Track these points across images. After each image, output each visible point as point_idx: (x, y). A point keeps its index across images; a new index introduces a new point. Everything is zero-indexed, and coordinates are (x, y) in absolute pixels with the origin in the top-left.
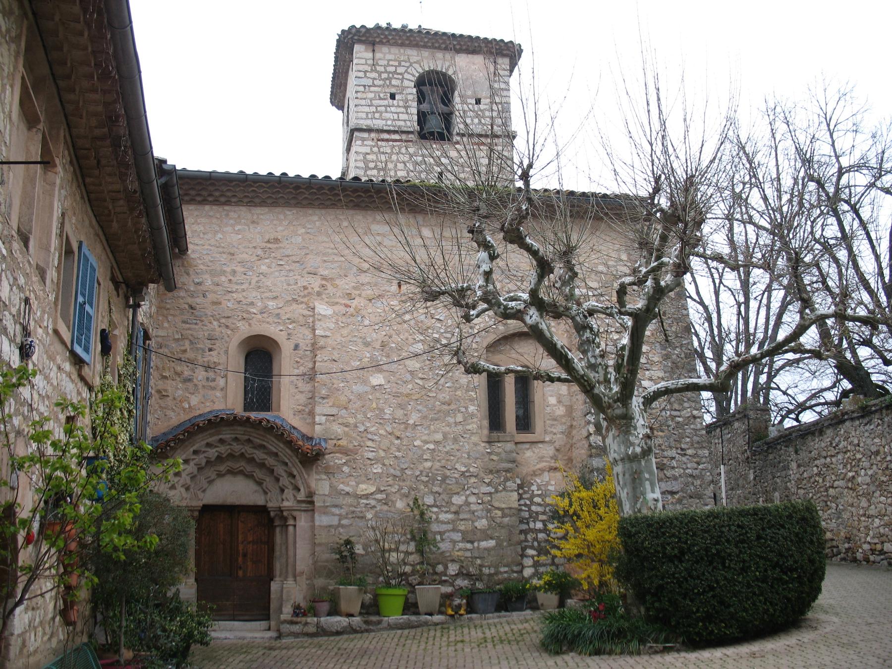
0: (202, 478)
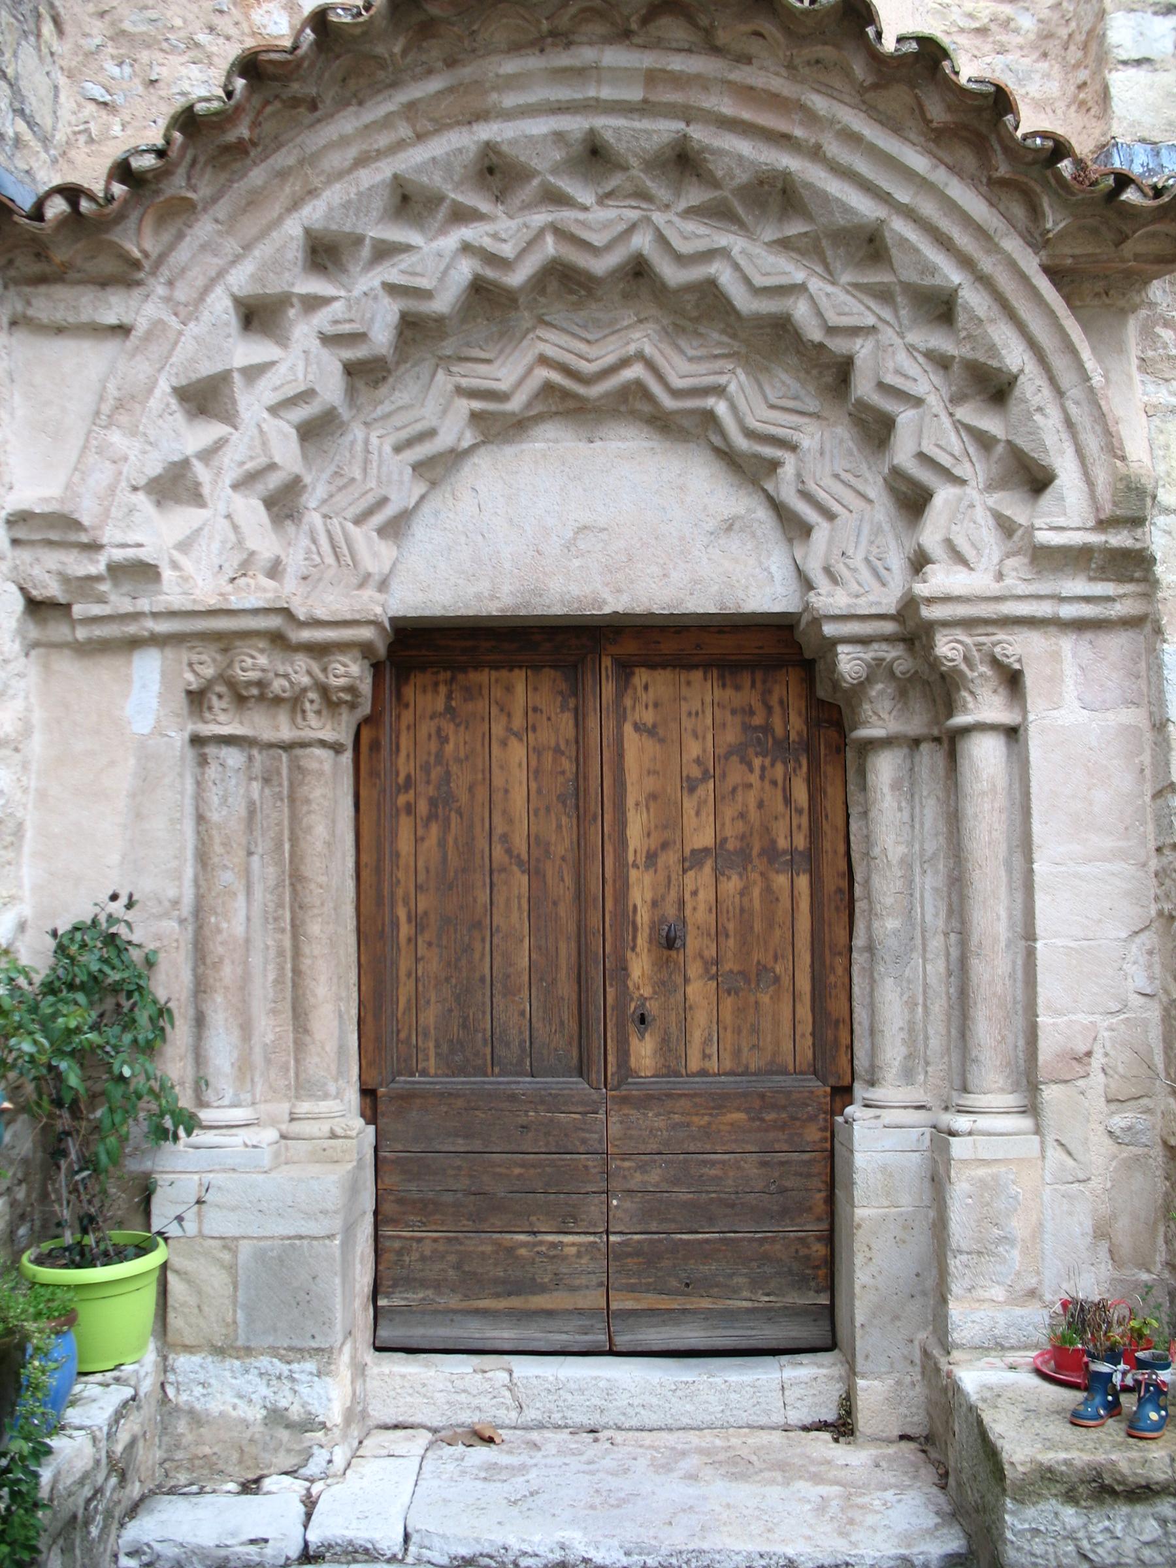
0: (381, 441)
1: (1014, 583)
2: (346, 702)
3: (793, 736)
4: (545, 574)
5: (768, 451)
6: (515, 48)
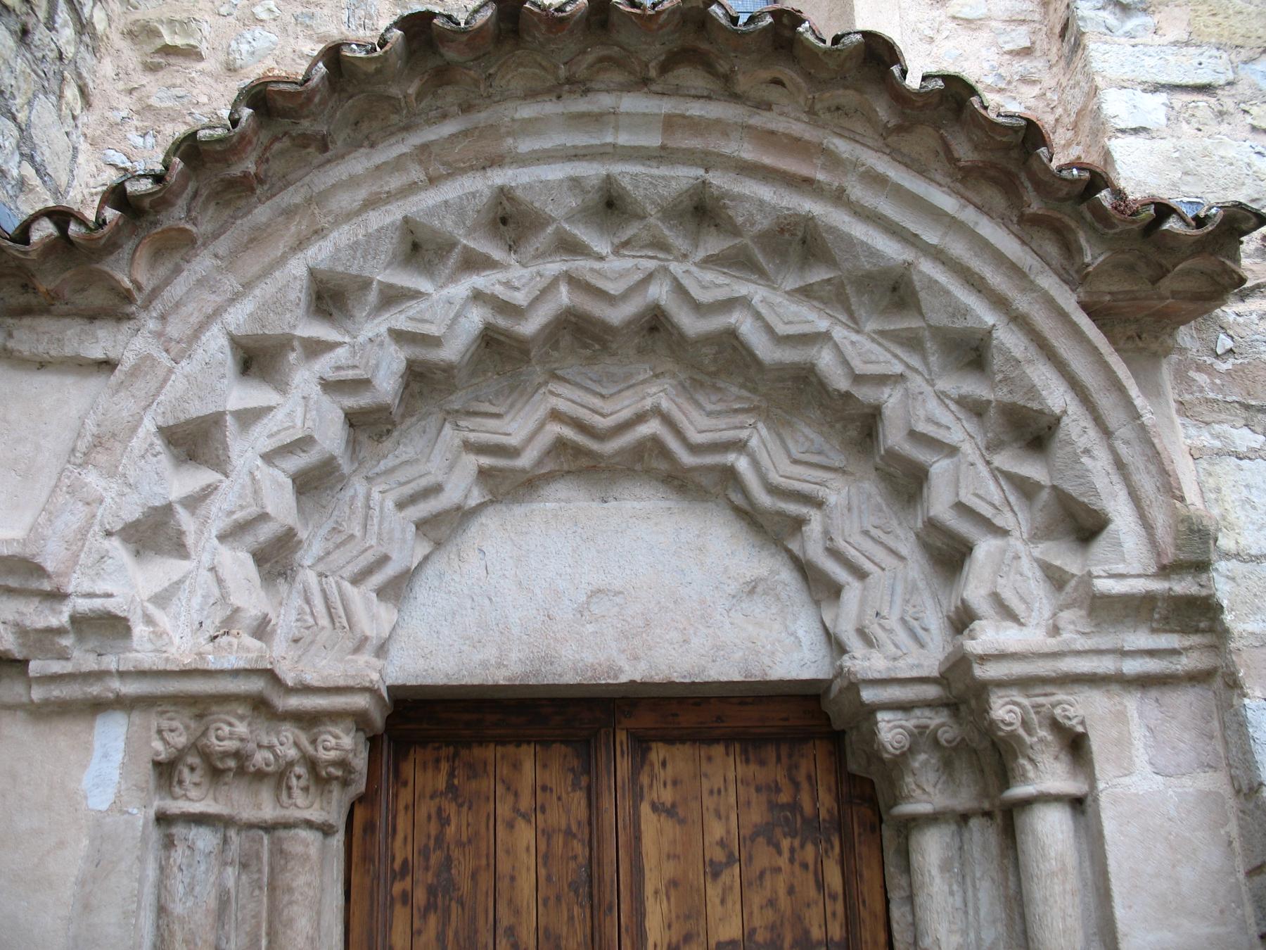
0: (383, 497)
1: (1071, 637)
2: (337, 778)
3: (823, 814)
4: (556, 639)
5: (793, 508)
6: (531, 95)
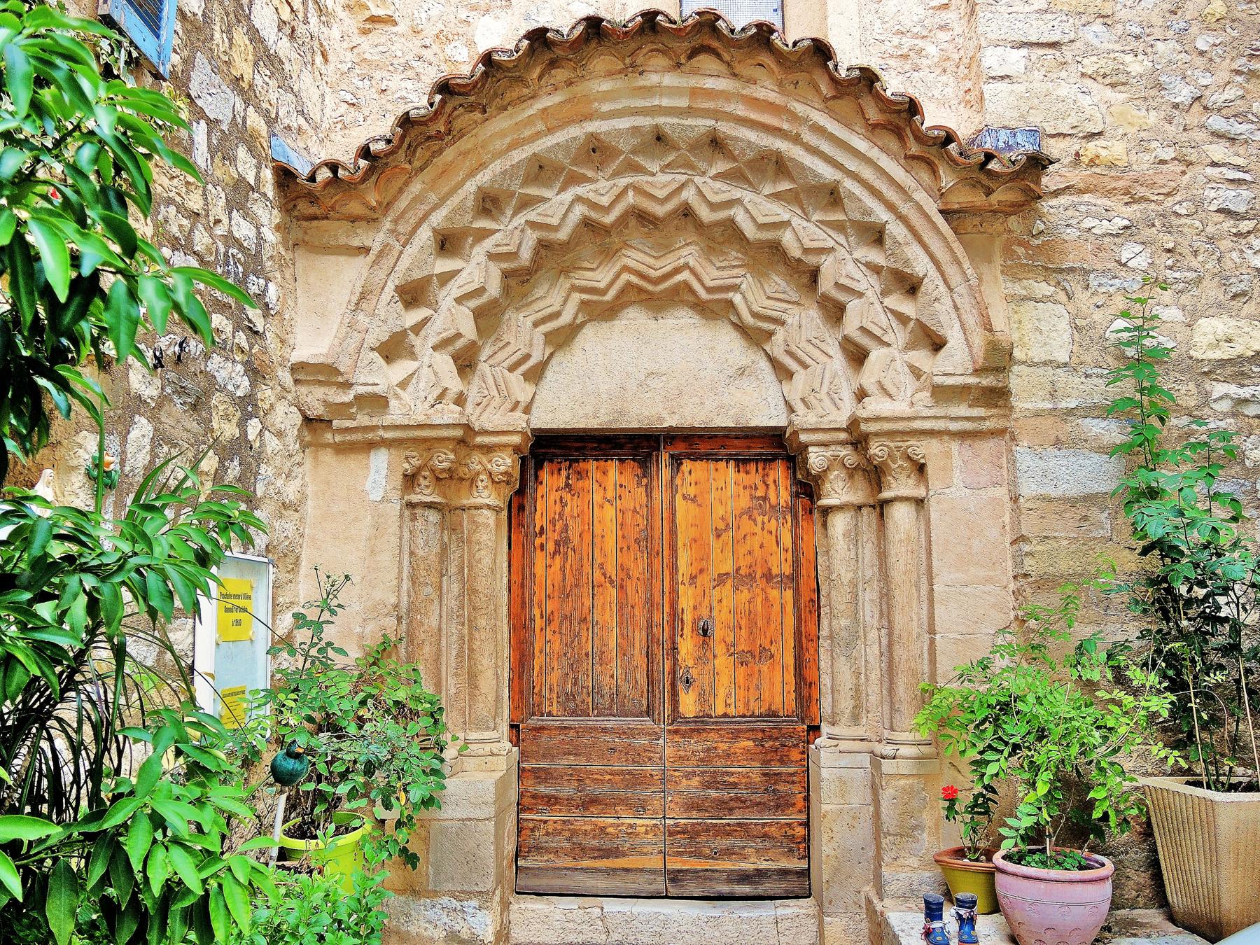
3: (782, 503)
6: (609, 74)
